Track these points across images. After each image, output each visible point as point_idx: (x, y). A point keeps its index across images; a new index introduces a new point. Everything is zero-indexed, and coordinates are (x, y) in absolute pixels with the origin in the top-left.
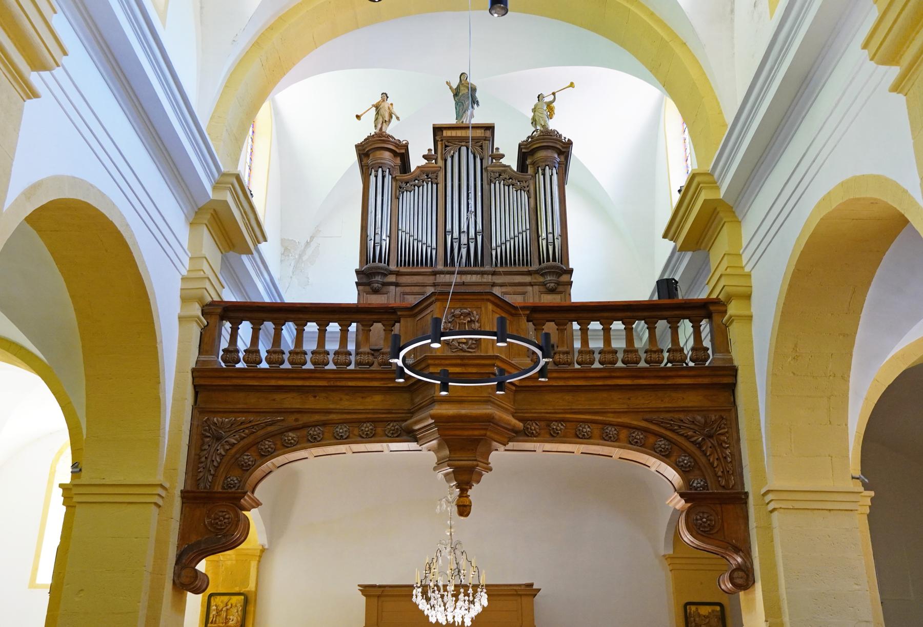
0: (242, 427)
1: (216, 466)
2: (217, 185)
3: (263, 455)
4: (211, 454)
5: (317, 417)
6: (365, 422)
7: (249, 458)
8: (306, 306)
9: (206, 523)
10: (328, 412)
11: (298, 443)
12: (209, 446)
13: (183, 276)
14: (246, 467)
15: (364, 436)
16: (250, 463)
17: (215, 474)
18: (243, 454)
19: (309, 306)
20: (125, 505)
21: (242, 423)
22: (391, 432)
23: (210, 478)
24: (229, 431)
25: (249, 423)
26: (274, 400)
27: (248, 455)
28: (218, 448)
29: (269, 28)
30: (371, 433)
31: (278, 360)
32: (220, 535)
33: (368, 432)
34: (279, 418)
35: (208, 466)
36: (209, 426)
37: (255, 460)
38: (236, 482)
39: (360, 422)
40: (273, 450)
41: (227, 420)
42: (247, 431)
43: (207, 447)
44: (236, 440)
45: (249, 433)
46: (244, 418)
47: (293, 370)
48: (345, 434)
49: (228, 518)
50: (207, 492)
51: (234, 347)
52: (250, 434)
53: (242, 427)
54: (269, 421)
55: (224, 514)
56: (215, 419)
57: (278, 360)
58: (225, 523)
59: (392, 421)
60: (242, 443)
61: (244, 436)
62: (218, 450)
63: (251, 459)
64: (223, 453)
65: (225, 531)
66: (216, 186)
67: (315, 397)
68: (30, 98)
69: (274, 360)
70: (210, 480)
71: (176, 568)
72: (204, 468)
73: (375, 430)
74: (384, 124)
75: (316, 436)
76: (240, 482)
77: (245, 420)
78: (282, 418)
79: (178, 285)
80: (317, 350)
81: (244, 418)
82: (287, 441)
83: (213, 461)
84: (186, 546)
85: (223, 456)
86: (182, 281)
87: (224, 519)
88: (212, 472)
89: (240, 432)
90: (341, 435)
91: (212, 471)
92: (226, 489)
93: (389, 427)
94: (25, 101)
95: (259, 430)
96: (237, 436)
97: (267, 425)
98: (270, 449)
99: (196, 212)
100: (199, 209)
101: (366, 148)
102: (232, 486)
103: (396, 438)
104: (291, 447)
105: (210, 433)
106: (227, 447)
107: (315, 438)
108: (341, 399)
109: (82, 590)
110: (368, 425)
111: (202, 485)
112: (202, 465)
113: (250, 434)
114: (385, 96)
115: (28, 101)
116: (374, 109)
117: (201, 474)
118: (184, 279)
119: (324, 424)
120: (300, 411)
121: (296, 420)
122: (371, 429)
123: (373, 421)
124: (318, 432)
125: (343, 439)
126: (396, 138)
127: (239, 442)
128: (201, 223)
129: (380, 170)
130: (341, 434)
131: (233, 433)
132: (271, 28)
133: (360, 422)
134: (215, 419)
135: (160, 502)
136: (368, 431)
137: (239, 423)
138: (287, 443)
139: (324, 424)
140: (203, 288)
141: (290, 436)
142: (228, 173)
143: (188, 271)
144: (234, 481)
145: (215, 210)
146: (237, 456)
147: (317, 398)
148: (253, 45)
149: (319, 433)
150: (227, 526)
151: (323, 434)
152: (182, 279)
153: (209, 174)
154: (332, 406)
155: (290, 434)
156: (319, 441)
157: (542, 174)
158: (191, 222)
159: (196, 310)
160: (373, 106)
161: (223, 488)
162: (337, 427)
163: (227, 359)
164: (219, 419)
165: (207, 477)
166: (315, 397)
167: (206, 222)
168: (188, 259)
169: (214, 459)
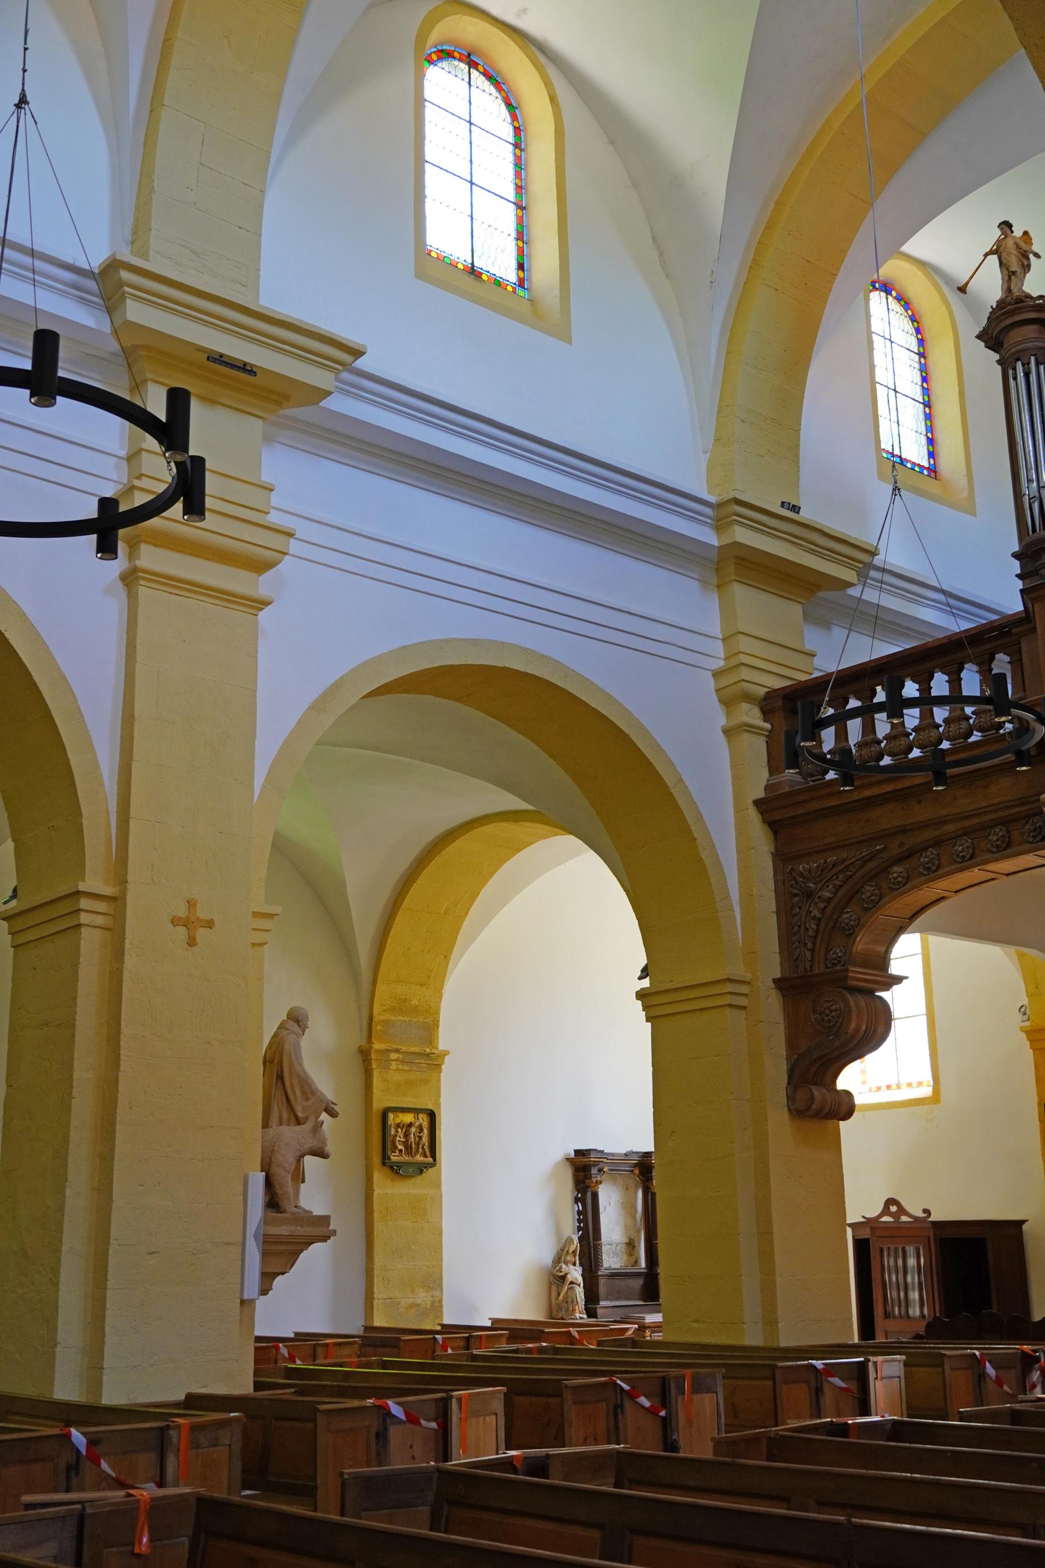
0: (834, 871)
1: (812, 935)
2: (720, 523)
3: (867, 909)
4: (803, 918)
5: (927, 834)
6: (992, 827)
7: (851, 916)
8: (883, 661)
9: (813, 1020)
10: (940, 822)
11: (908, 879)
12: (800, 908)
13: (713, 671)
14: (850, 930)
15: (994, 849)
16: (852, 923)
17: (814, 948)
18: (842, 913)
19: (885, 660)
20: (699, 1013)
21: (833, 865)
22: (1032, 834)
23: (808, 955)
24: (820, 881)
25: (842, 863)
26: (868, 820)
27: (848, 912)
28: (811, 909)
29: (766, 227)
30: (1003, 842)
31: (871, 756)
32: (832, 1035)
33: (998, 843)
34: (878, 848)
35: (802, 938)
36: (795, 879)
37: (859, 919)
38: (839, 955)
39: (986, 828)
40: (878, 898)
41: (815, 865)
42: (841, 876)
43: (797, 910)
44: (830, 891)
45: (845, 880)
46: (835, 858)
47: (986, 740)
48: (968, 852)
49: (836, 1010)
50: (800, 978)
51: (819, 751)
52: (847, 880)
53: (834, 871)
54: (867, 855)
55: (830, 1004)
56: (801, 868)
57: (871, 756)
58: (832, 1017)
59: (1029, 816)
60: (839, 895)
61: (840, 884)
62: (811, 912)
63: (853, 917)
64: (818, 915)
65: (836, 1028)
66: (720, 525)
67: (920, 802)
68: (261, 609)
69: (866, 757)
70: (809, 958)
71: (789, 1089)
72: (799, 942)
73: (1009, 837)
74: (1013, 277)
75: (929, 865)
76: (845, 954)
77: (836, 860)
78: (882, 846)
79: (711, 684)
80: (864, 739)
81: (835, 858)
82: (892, 880)
83: (807, 929)
84: (796, 1056)
85: (819, 919)
86: (714, 679)
87: (831, 1012)
88: (810, 946)
89: (834, 880)
90: (962, 856)
91: (809, 944)
92: (829, 968)
93: (1027, 827)
94: (257, 615)
95: (857, 871)
96: (831, 887)
97: (864, 862)
98: (873, 898)
99: (717, 569)
100: (718, 563)
101: (992, 333)
102: (836, 962)
103: (1040, 843)
104: (900, 888)
105: (797, 888)
106: (822, 905)
107: (929, 869)
108: (955, 798)
109: (673, 1132)
110: (997, 830)
111: (801, 967)
112: (796, 937)
113: (847, 880)
114: (1006, 226)
115: (261, 614)
116: (994, 259)
117: (798, 951)
118: (716, 674)
119: (937, 843)
120: (903, 830)
121: (901, 845)
122: (1002, 836)
123: (1004, 822)
124: (931, 857)
125: (966, 861)
126: (1035, 295)
127: (835, 894)
128: (728, 582)
129: (1019, 365)
130: (961, 854)
131: (826, 882)
132: (769, 227)
133: (986, 828)
134: (801, 868)
135: (742, 1001)
136: (998, 840)
137: (831, 867)
138: (894, 883)
139: (937, 843)
140: (739, 681)
141: (896, 872)
142: (721, 502)
143: (726, 659)
144: (837, 954)
145: (736, 557)
146: (835, 916)
147: (923, 804)
148: (750, 267)
149: (933, 859)
150: (837, 1022)
151: (939, 860)
152: (713, 675)
153: (694, 517)
154: (944, 812)
155: (896, 869)
156: (935, 871)
157: (1013, 378)
158: (716, 585)
159: (752, 715)
160: (991, 252)
161: (827, 967)
162: (955, 844)
163: (809, 770)
164: (806, 866)
165: (805, 955)
166: (920, 802)
167: (733, 577)
168: (720, 642)
169: (808, 926)
